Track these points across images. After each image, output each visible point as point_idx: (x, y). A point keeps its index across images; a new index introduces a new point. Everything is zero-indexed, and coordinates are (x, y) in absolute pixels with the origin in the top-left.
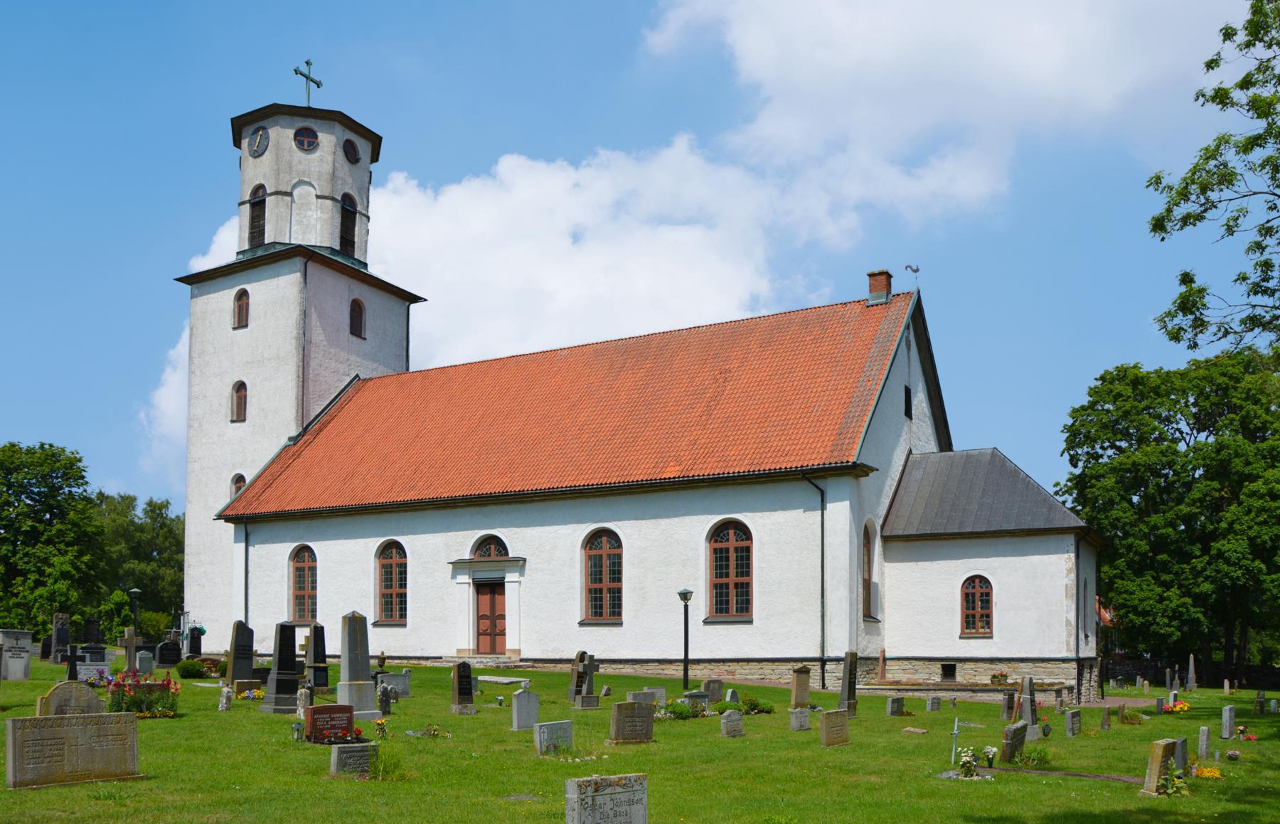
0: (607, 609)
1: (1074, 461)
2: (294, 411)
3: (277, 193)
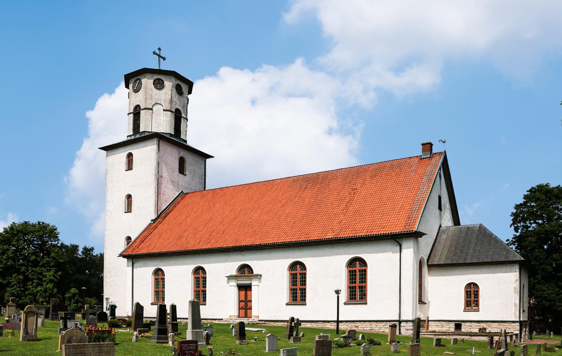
0: (299, 298)
1: (516, 230)
3: (145, 109)
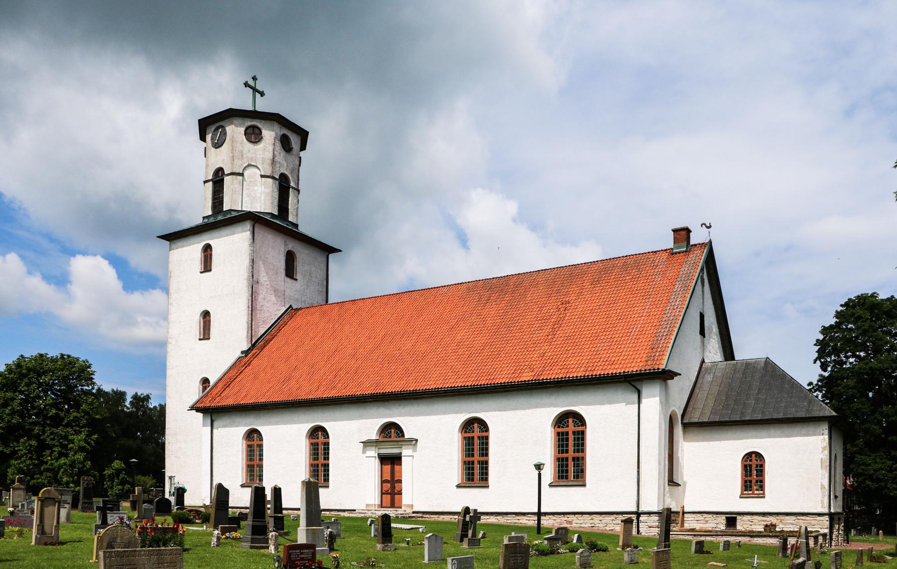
0: (477, 476)
1: (824, 367)
2: (245, 332)
